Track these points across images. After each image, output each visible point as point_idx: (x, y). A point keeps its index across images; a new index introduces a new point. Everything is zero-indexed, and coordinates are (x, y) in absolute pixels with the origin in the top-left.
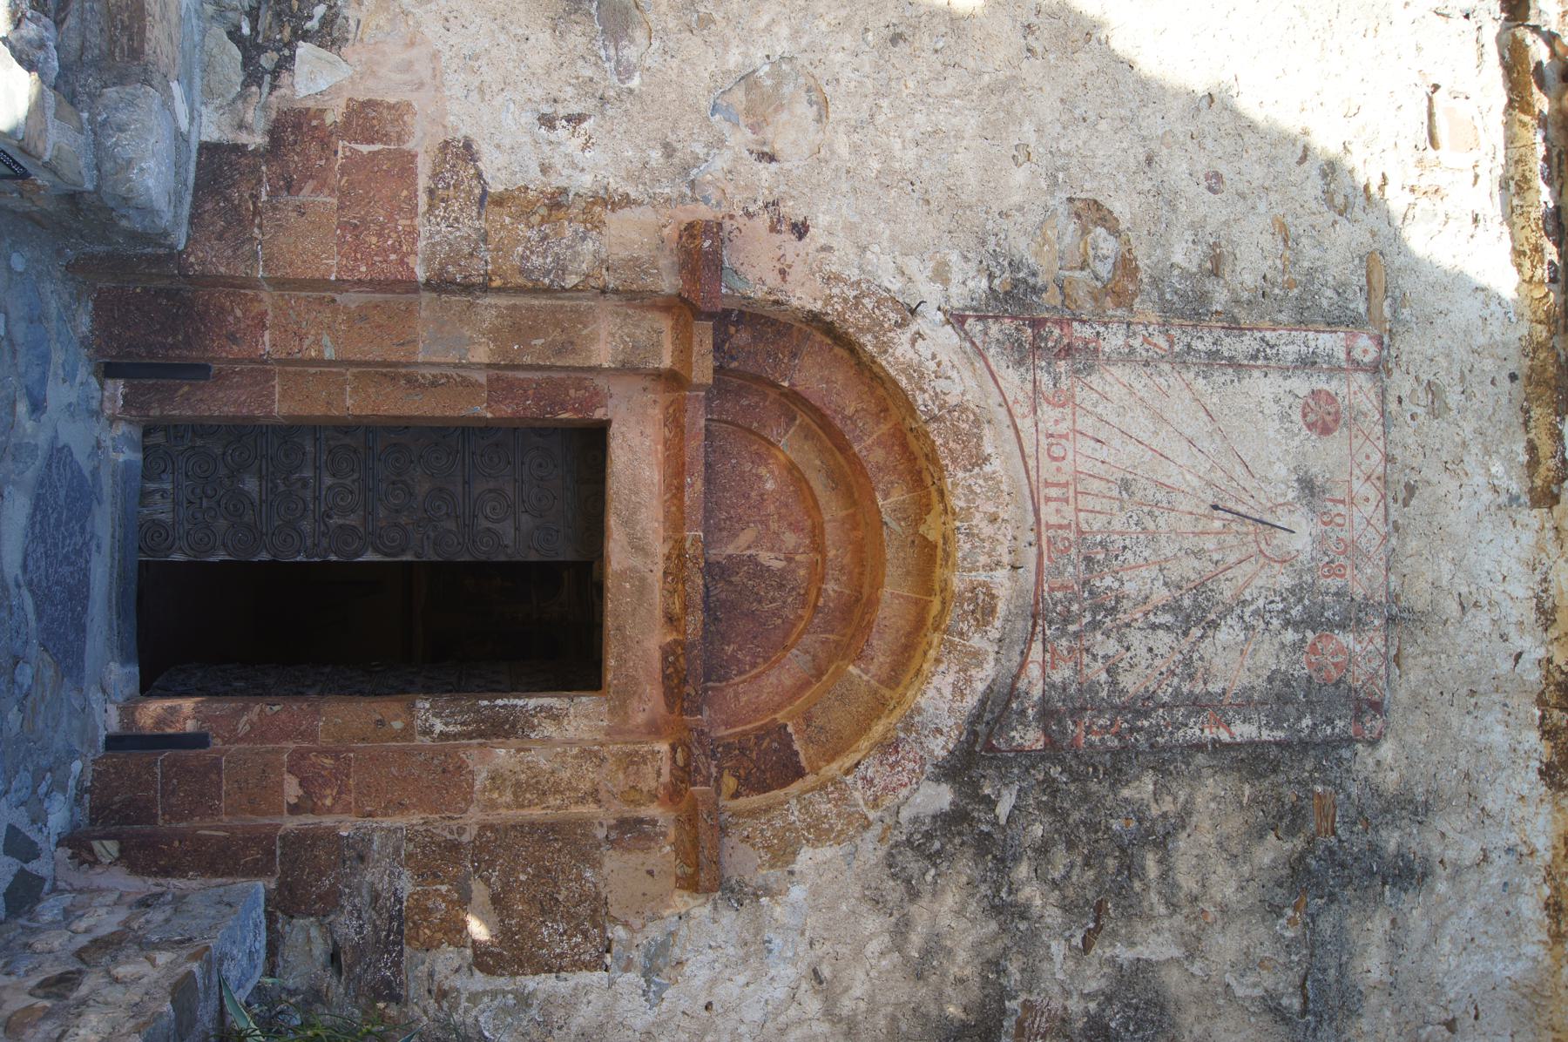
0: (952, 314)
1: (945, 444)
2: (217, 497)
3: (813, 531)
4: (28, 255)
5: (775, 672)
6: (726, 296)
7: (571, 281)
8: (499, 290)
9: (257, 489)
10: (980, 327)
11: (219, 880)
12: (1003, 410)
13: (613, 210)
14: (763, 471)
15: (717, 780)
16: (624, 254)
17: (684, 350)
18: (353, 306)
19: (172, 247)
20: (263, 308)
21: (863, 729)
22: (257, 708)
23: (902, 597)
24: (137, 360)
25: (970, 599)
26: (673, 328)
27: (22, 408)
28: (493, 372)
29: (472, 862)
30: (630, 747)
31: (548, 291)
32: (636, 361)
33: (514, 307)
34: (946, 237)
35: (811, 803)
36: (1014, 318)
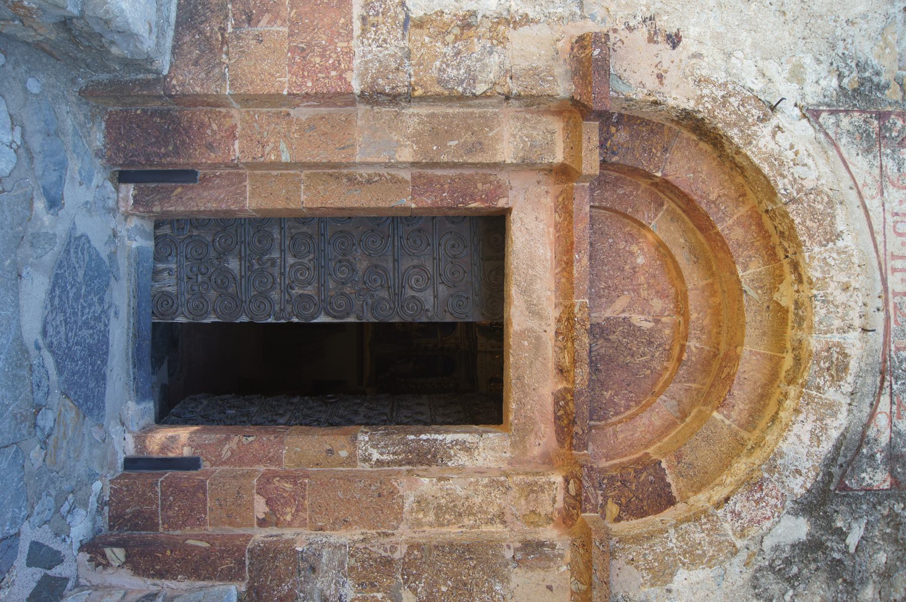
0: (807, 110)
1: (803, 223)
2: (209, 274)
3: (676, 297)
4: (44, 81)
5: (646, 414)
6: (612, 99)
7: (480, 89)
8: (422, 99)
9: (238, 267)
10: (832, 120)
11: (201, 583)
12: (854, 193)
13: (515, 28)
14: (634, 248)
15: (603, 506)
16: (525, 65)
17: (574, 146)
18: (304, 119)
19: (158, 72)
20: (233, 122)
21: (725, 465)
22: (236, 439)
23: (759, 353)
24: (141, 168)
25: (826, 357)
26: (564, 129)
27: (40, 205)
28: (416, 171)
29: (403, 575)
30: (531, 479)
31: (461, 98)
32: (534, 158)
33: (433, 115)
34: (801, 43)
35: (687, 532)
36: (862, 111)
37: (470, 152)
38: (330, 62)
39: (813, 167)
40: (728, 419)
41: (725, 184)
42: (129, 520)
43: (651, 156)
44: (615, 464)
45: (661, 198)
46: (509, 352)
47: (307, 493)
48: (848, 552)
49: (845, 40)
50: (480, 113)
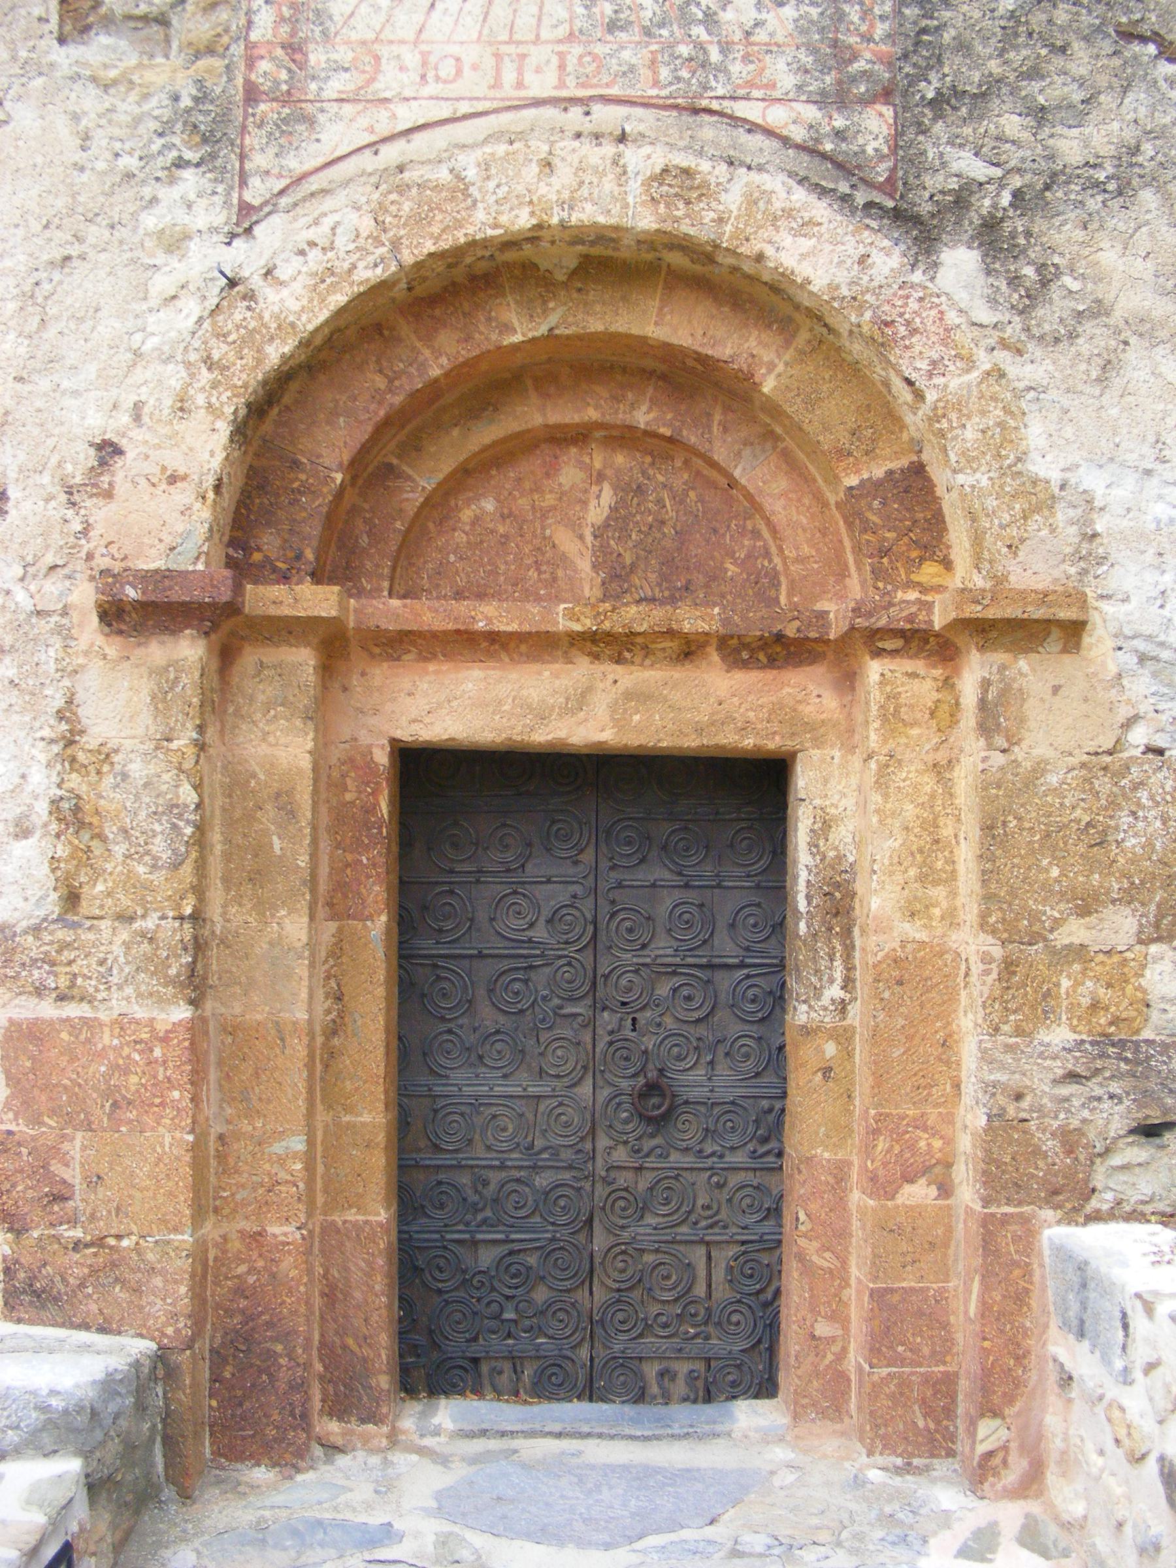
0: (237, 224)
5: (768, 504)
7: (188, 795)
10: (255, 182)
15: (924, 590)
25: (667, 206)
31: (201, 829)
33: (226, 880)
35: (963, 453)
37: (292, 814)
38: (137, 1057)
39: (336, 217)
40: (775, 366)
41: (358, 360)
42: (938, 1422)
43: (305, 490)
44: (855, 561)
45: (378, 468)
46: (653, 748)
47: (894, 1112)
48: (1001, 179)
49: (117, 155)
50: (223, 794)
